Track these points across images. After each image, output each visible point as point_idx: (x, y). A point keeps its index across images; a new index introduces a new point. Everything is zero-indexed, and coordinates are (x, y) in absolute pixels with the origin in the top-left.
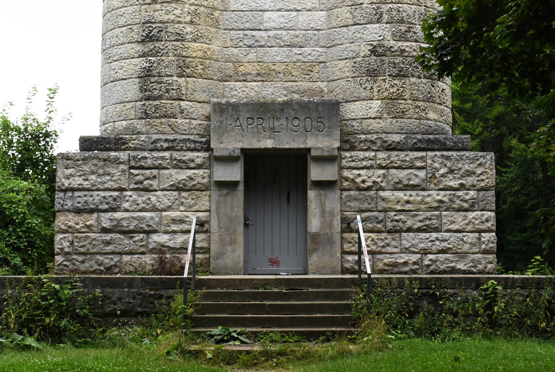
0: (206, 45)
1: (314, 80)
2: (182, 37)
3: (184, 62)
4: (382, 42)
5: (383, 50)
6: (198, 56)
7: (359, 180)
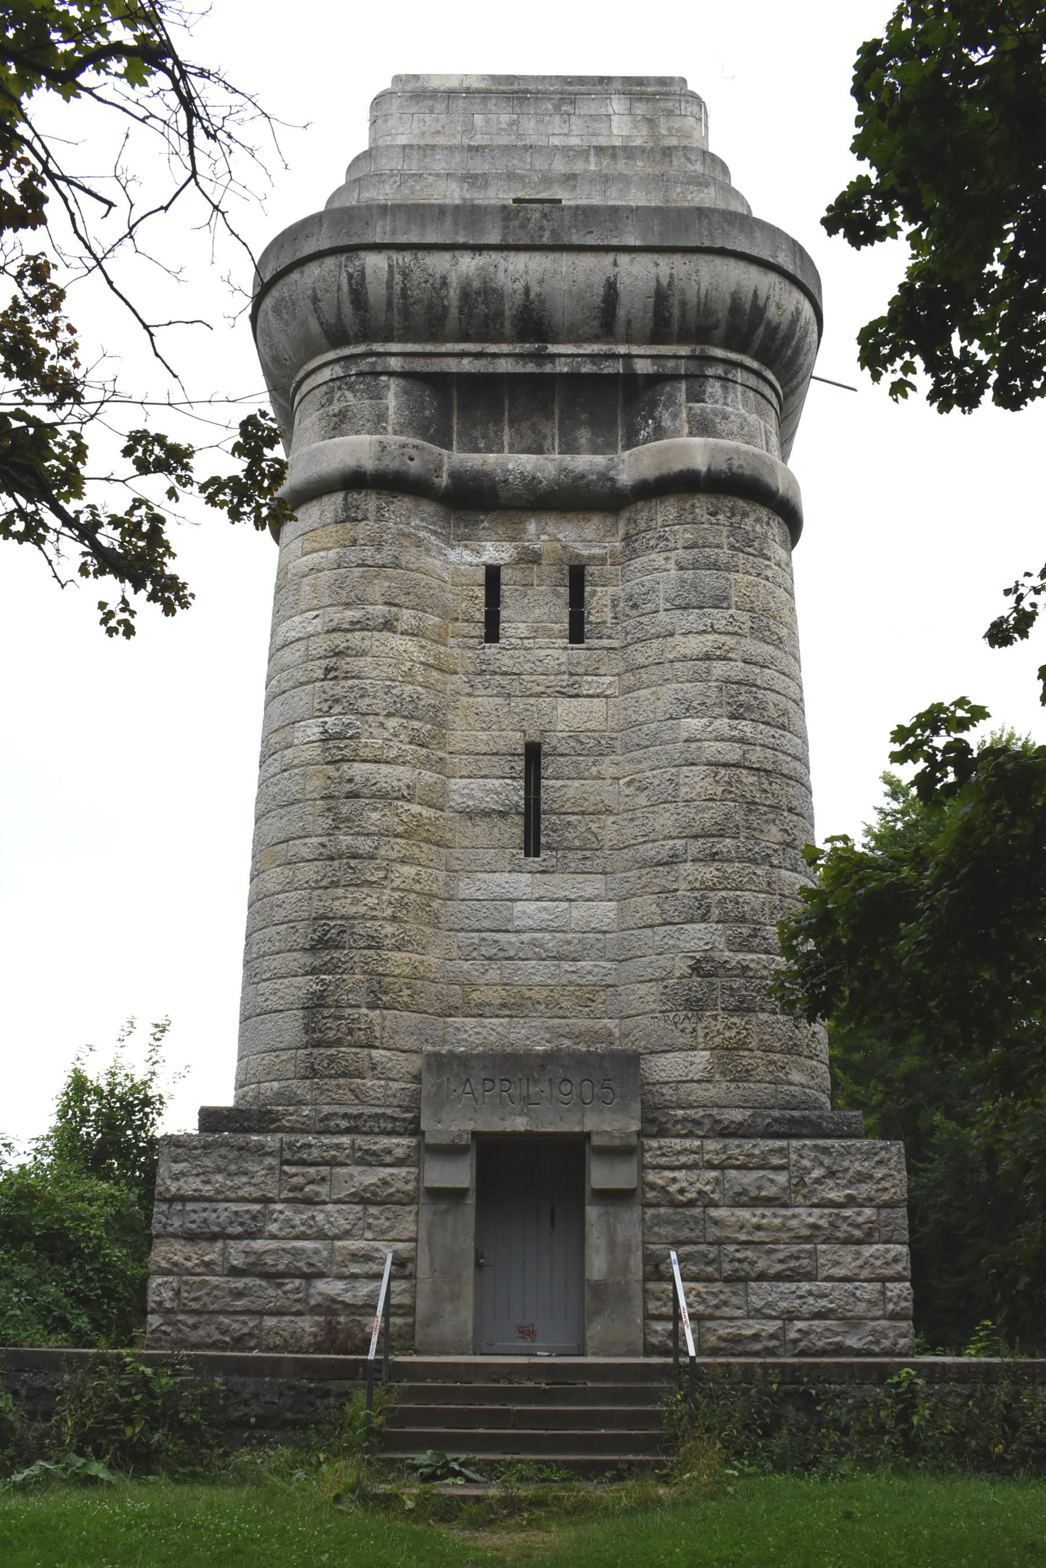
7: (673, 1188)
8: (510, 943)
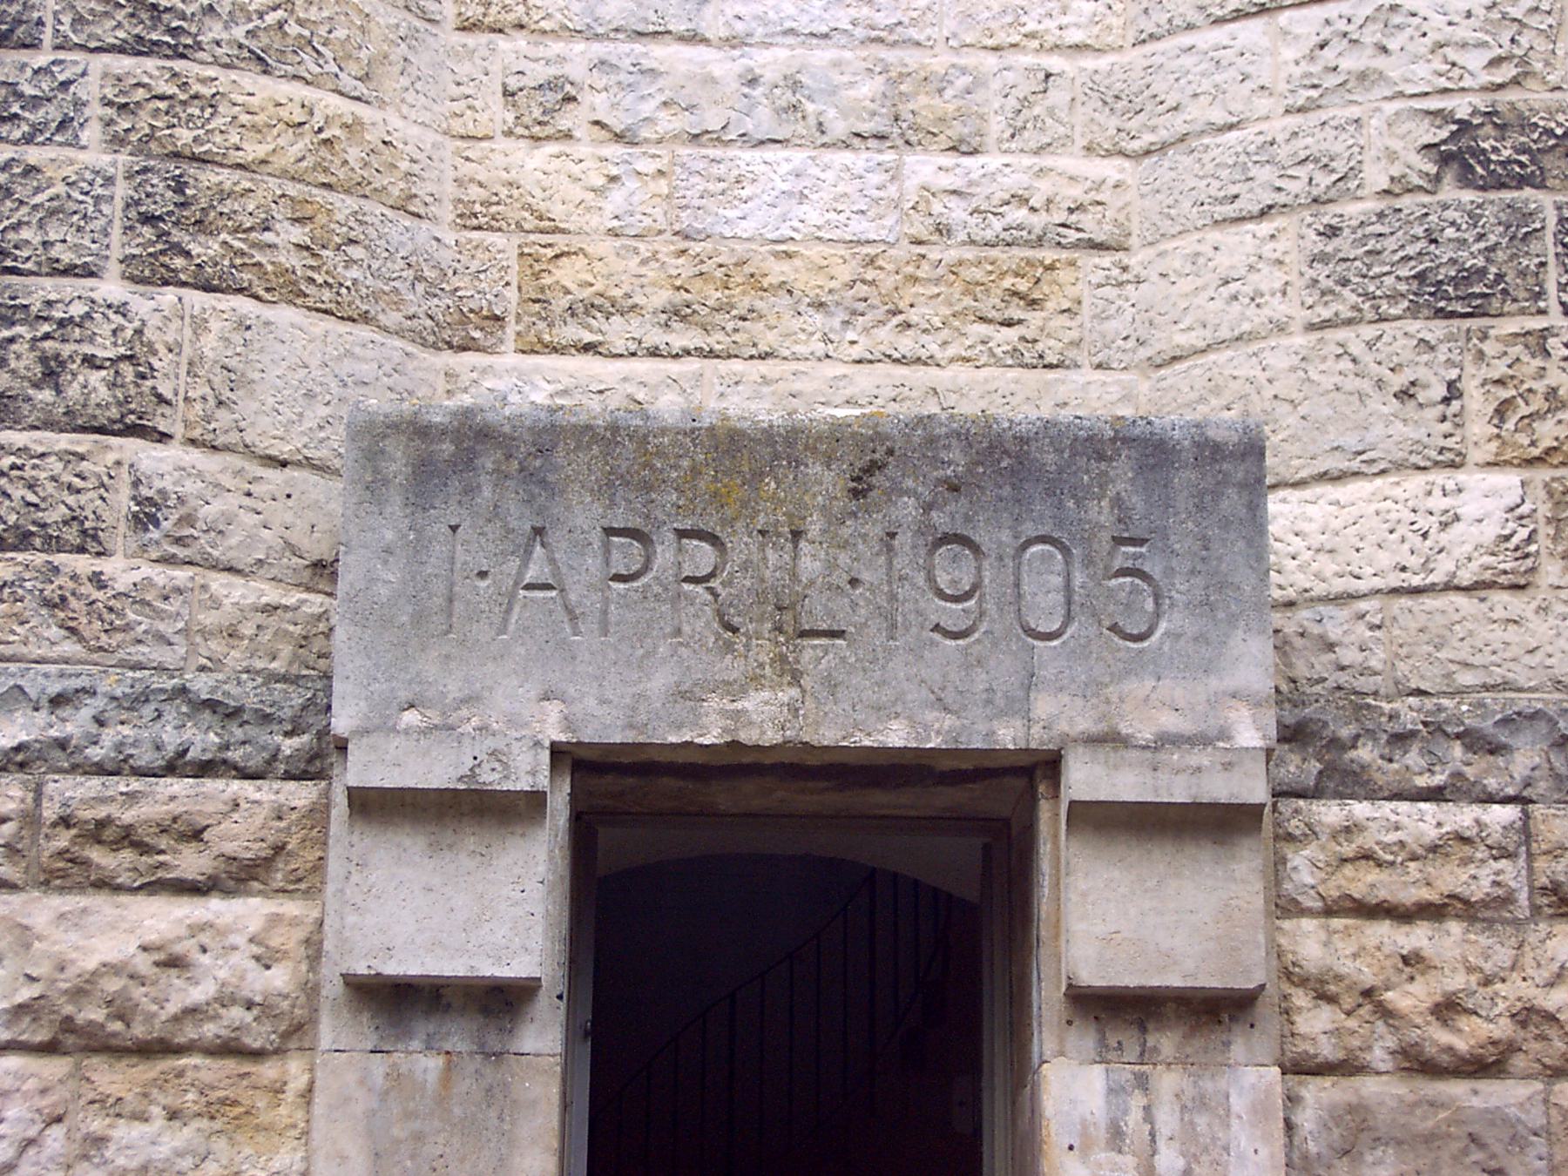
0: (335, 100)
1: (1051, 358)
2: (173, 32)
3: (180, 187)
4: (1511, 95)
5: (1524, 150)
6: (278, 162)
7: (1410, 998)
8: (711, 80)
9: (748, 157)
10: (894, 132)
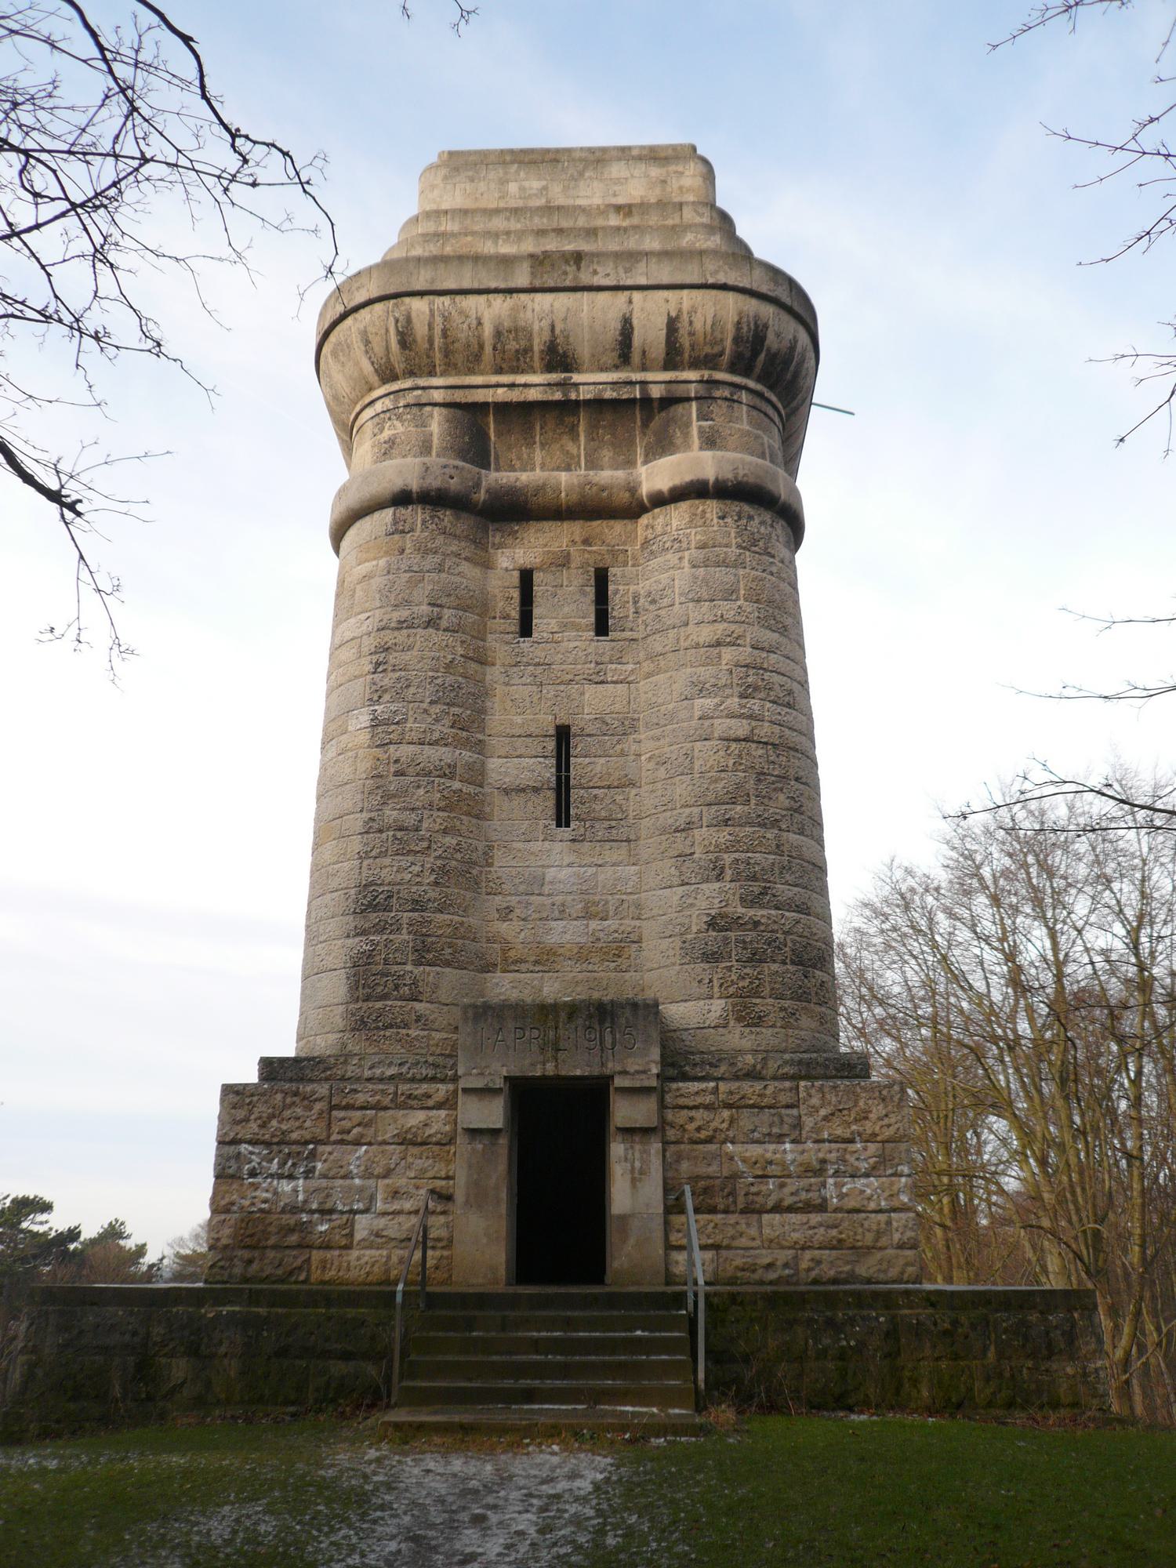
9: (553, 924)
10: (588, 915)
